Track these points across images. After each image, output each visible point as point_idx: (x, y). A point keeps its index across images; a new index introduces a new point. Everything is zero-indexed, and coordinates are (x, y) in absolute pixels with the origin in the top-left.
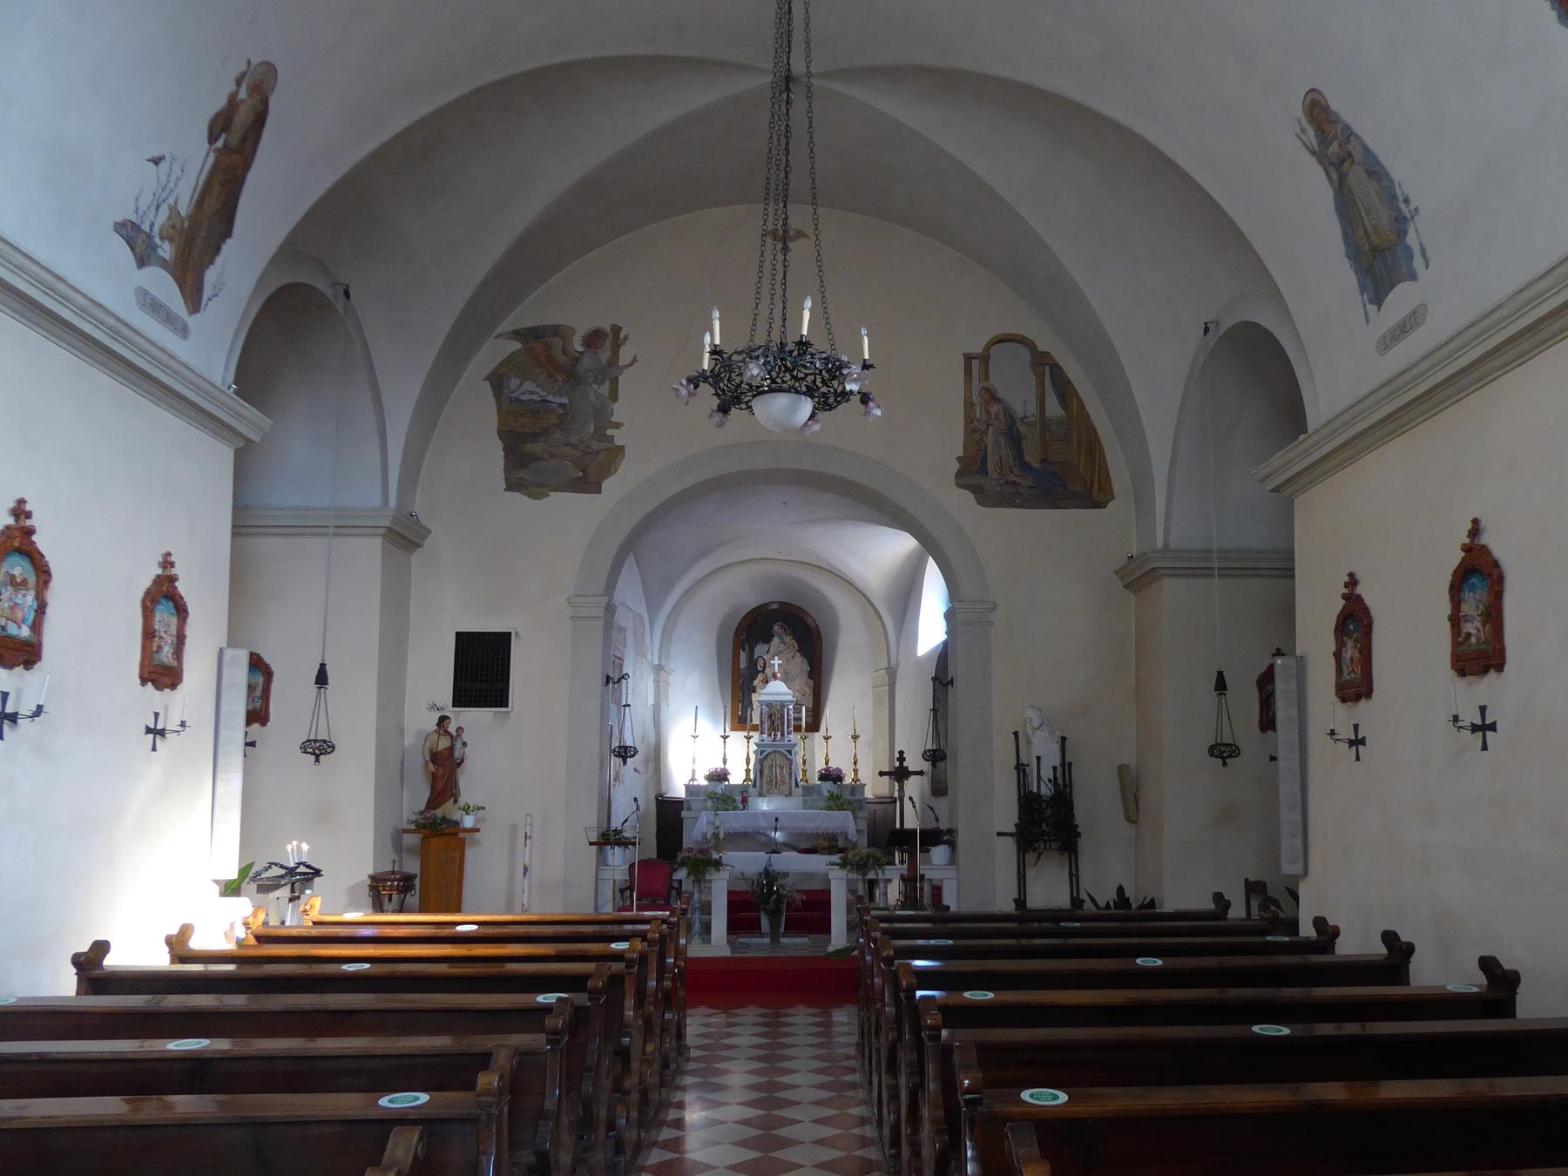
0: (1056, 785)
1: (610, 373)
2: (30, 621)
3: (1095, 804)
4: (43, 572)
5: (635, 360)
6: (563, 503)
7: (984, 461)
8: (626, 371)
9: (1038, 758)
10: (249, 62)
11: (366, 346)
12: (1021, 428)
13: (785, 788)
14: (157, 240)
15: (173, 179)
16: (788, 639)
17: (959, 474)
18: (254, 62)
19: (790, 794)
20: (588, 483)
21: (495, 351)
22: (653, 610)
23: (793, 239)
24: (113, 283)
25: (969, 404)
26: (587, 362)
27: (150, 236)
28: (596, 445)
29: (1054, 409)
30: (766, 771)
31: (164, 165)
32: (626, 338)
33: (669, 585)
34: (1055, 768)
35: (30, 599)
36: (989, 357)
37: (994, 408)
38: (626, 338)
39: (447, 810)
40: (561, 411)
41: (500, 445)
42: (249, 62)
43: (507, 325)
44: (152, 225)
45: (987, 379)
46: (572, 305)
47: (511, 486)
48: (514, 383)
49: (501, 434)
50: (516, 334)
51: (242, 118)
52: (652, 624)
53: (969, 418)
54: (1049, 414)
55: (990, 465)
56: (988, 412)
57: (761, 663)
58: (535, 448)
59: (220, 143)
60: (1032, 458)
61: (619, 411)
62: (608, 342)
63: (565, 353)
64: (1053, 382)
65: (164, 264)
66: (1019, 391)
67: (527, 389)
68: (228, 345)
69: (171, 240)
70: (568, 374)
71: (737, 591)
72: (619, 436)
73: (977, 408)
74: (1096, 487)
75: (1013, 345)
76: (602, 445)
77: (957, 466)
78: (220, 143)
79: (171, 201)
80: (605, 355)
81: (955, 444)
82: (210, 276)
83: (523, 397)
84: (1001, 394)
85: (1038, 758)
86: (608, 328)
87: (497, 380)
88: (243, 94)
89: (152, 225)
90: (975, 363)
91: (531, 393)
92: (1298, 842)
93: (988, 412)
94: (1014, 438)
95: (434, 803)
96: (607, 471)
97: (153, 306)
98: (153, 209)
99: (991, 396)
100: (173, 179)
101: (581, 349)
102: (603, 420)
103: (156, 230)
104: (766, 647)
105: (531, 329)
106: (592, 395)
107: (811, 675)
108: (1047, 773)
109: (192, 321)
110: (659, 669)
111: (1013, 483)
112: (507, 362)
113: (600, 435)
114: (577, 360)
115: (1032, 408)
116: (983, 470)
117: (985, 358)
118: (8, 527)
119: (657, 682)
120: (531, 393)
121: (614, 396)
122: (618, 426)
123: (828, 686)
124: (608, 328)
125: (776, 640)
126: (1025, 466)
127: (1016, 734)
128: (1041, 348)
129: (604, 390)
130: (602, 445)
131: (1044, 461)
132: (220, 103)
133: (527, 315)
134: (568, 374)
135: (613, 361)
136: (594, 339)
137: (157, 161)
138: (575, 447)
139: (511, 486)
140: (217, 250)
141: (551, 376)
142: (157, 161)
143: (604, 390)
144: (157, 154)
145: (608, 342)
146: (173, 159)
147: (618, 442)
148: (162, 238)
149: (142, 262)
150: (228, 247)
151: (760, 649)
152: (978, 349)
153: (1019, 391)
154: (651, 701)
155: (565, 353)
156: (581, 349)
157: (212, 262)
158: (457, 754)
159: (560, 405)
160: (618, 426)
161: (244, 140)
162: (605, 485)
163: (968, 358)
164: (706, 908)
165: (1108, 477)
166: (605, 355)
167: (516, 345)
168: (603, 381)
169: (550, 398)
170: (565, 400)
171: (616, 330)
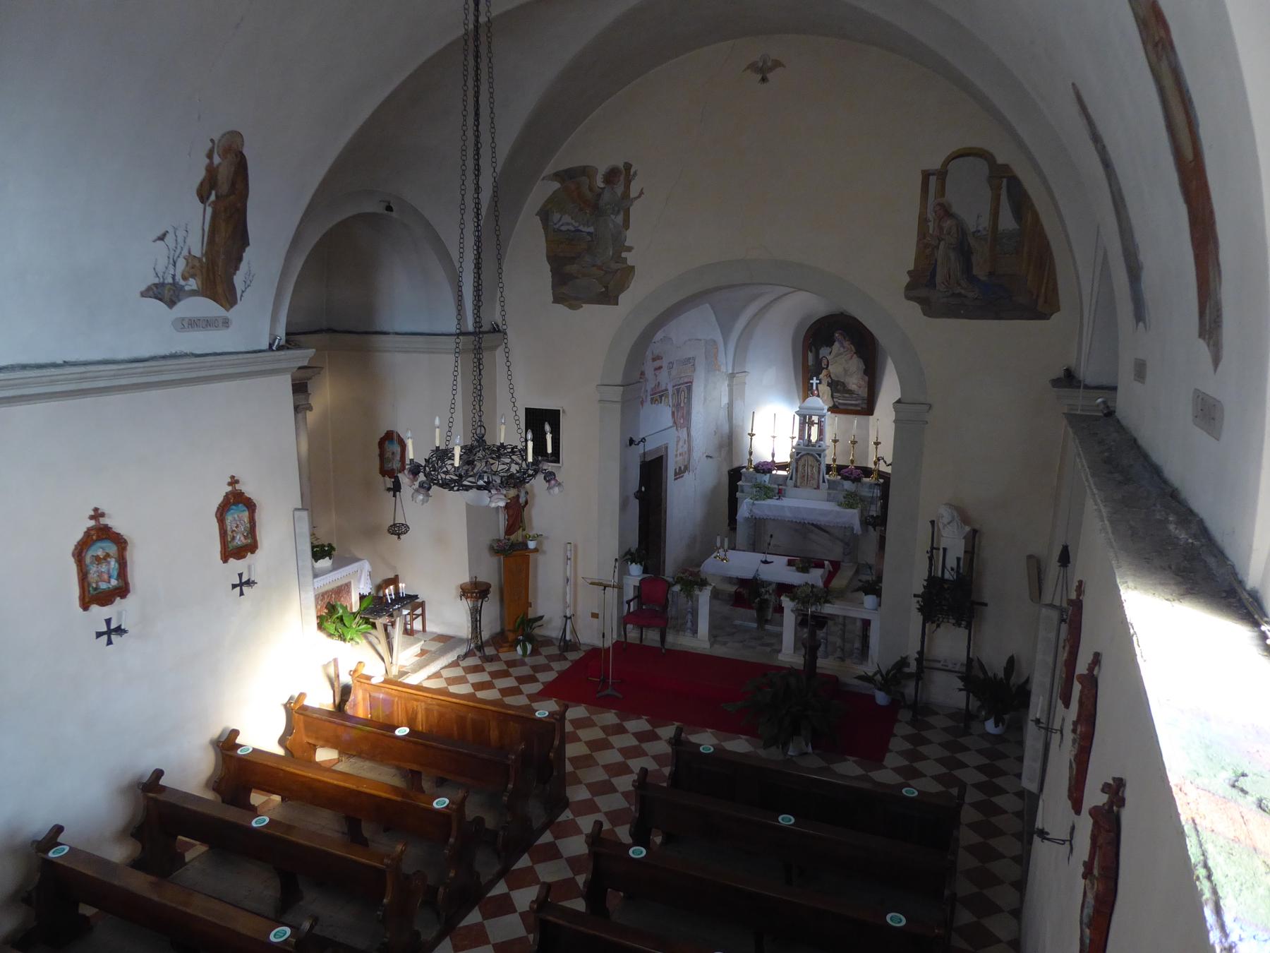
0: (958, 572)
1: (624, 205)
2: (115, 574)
3: (1002, 581)
4: (121, 543)
5: (641, 193)
6: (592, 312)
7: (933, 275)
8: (636, 203)
9: (945, 550)
10: (212, 140)
11: (428, 225)
12: (972, 242)
13: (815, 482)
14: (182, 283)
15: (180, 240)
16: (846, 344)
17: (909, 287)
18: (216, 137)
19: (818, 487)
20: (609, 297)
21: (542, 191)
22: (726, 333)
23: (771, 69)
24: (154, 329)
25: (923, 221)
26: (607, 196)
27: (174, 284)
28: (614, 266)
29: (1007, 222)
30: (800, 469)
31: (170, 239)
32: (635, 173)
33: (735, 316)
34: (958, 559)
35: (113, 564)
36: (946, 172)
37: (948, 224)
38: (635, 173)
39: (517, 536)
40: (589, 238)
41: (548, 267)
42: (212, 140)
43: (549, 169)
44: (174, 276)
45: (943, 195)
46: (594, 150)
47: (557, 300)
48: (556, 216)
49: (549, 258)
50: (558, 176)
51: (224, 175)
52: (725, 344)
53: (922, 234)
54: (1001, 227)
55: (939, 279)
56: (941, 228)
57: (824, 362)
58: (572, 268)
59: (213, 198)
60: (980, 271)
61: (631, 237)
62: (622, 178)
63: (591, 189)
64: (1010, 195)
65: (193, 293)
66: (973, 205)
67: (565, 222)
68: (270, 307)
69: (193, 276)
70: (593, 206)
71: (803, 305)
72: (631, 259)
73: (931, 225)
74: (1041, 300)
75: (971, 158)
76: (619, 266)
77: (907, 279)
78: (213, 198)
79: (185, 253)
80: (619, 190)
81: (906, 257)
82: (238, 280)
83: (563, 228)
84: (955, 209)
85: (945, 550)
86: (621, 166)
87: (545, 215)
88: (217, 160)
89: (174, 276)
90: (933, 179)
91: (568, 224)
92: (1038, 765)
93: (941, 228)
94: (964, 250)
95: (510, 530)
96: (622, 287)
97: (194, 323)
98: (171, 266)
99: (945, 212)
100: (180, 240)
101: (602, 185)
102: (620, 246)
103: (178, 277)
104: (828, 350)
105: (566, 171)
106: (611, 226)
107: (866, 372)
108: (951, 562)
109: (233, 314)
110: (732, 376)
111: (960, 295)
112: (550, 200)
113: (618, 259)
114: (599, 195)
115: (985, 222)
116: (931, 283)
117: (942, 174)
118: (89, 529)
119: (730, 386)
120: (568, 224)
121: (626, 224)
122: (629, 249)
123: (881, 380)
124: (621, 166)
125: (837, 344)
126: (972, 279)
127: (933, 522)
128: (1001, 160)
129: (619, 219)
130: (619, 266)
131: (991, 274)
132: (200, 174)
133: (563, 160)
134: (593, 206)
135: (626, 195)
136: (612, 176)
137: (162, 238)
138: (600, 268)
139: (557, 300)
140: (240, 259)
141: (581, 210)
142: (162, 238)
143: (619, 219)
144: (159, 233)
145: (622, 178)
146: (175, 229)
147: (630, 263)
148: (185, 278)
149: (171, 303)
150: (248, 254)
151: (824, 351)
152: (935, 163)
153: (973, 205)
154: (725, 400)
155: (591, 189)
156: (602, 185)
157: (237, 268)
158: (522, 500)
159: (589, 233)
160: (629, 249)
161: (233, 184)
162: (622, 297)
163: (926, 175)
164: (695, 613)
165: (1055, 290)
166: (619, 190)
167: (556, 185)
168: (618, 212)
169: (581, 228)
170: (591, 229)
171: (628, 166)
